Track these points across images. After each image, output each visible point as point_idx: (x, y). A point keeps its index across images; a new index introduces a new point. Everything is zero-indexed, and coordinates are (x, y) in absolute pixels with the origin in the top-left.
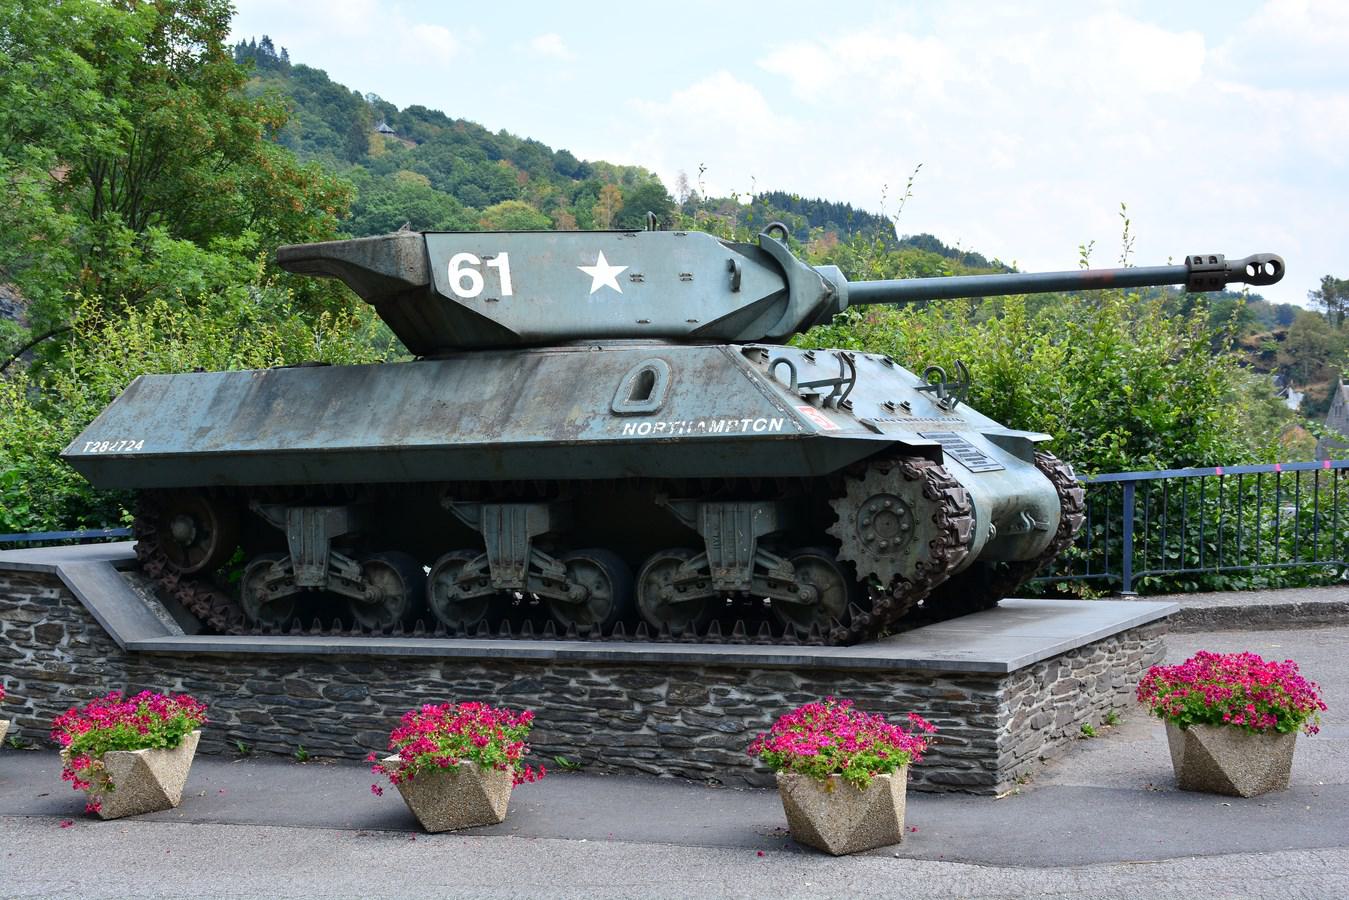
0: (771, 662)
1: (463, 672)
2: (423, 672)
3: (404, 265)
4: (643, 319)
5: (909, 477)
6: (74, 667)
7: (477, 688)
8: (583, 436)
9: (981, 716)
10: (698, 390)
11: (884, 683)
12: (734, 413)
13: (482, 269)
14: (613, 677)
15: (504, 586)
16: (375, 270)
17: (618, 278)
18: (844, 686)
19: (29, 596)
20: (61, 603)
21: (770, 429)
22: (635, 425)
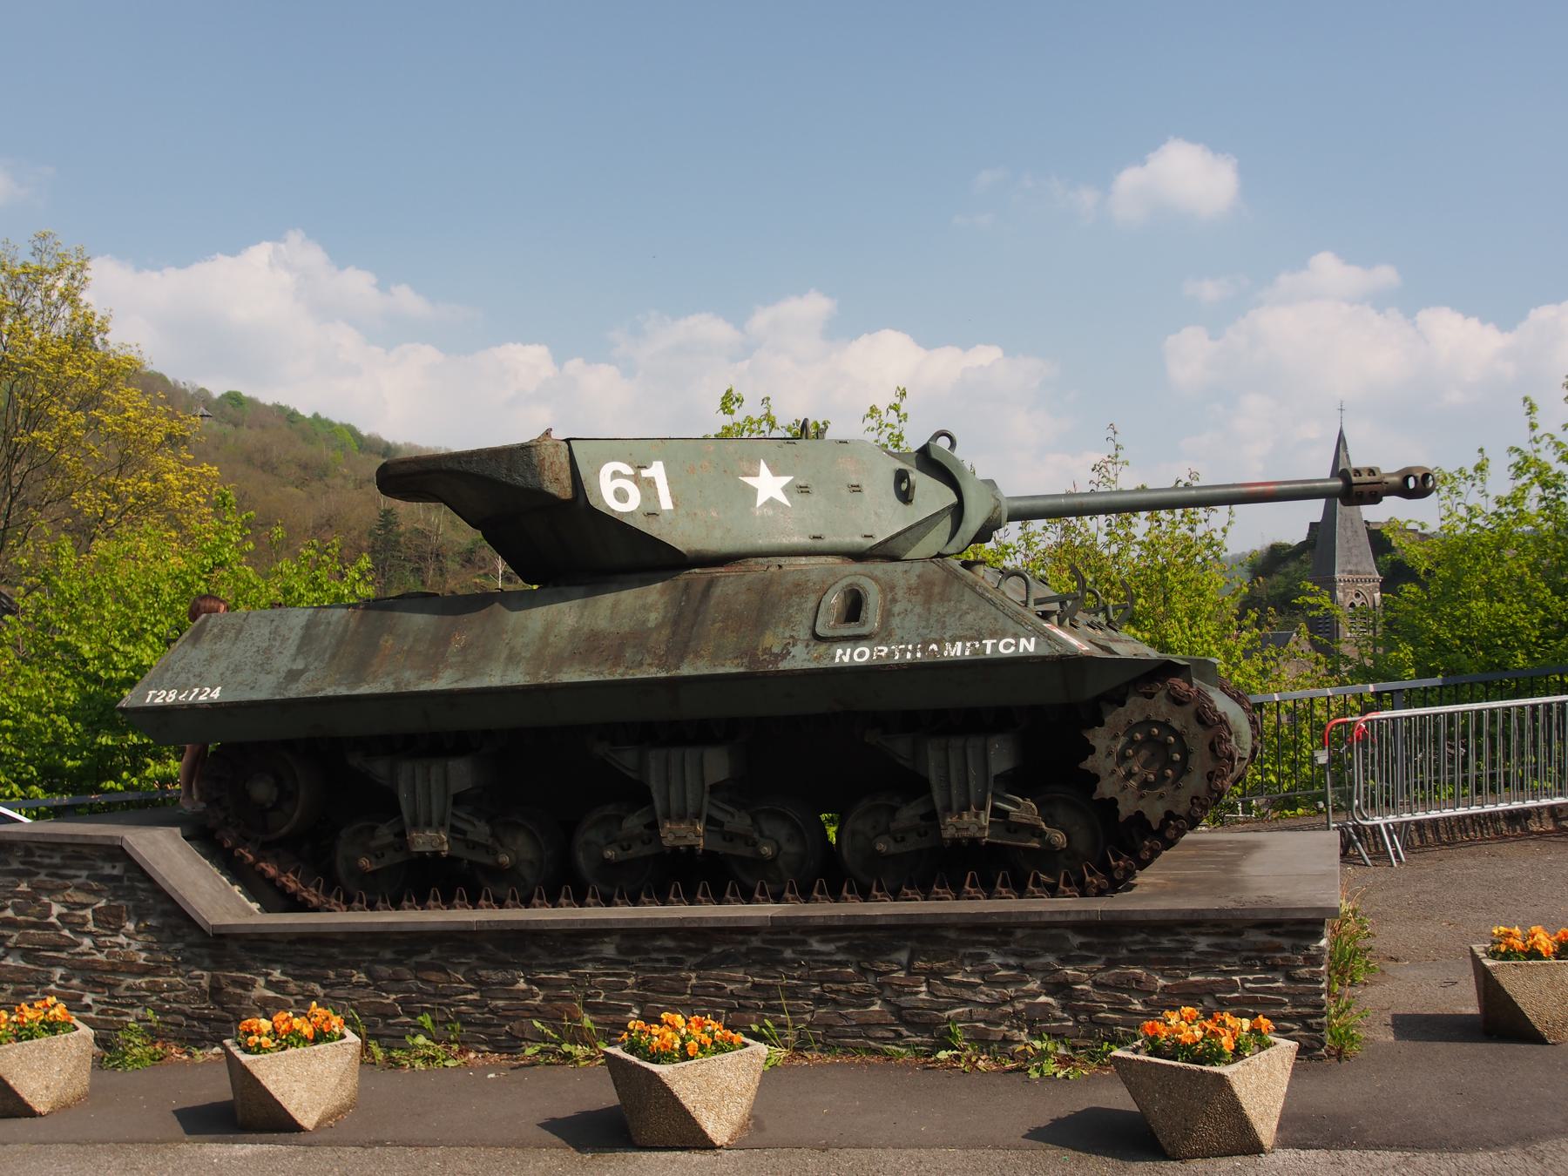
0: (1046, 918)
1: (646, 946)
2: (594, 948)
3: (548, 476)
4: (817, 534)
5: (1177, 701)
6: (144, 955)
7: (665, 965)
8: (784, 665)
9: (1304, 970)
10: (918, 609)
11: (1184, 937)
12: (969, 633)
13: (636, 479)
14: (839, 944)
15: (677, 843)
16: (512, 483)
17: (786, 490)
18: (1135, 943)
19: (85, 873)
20: (125, 879)
21: (1021, 650)
22: (849, 651)
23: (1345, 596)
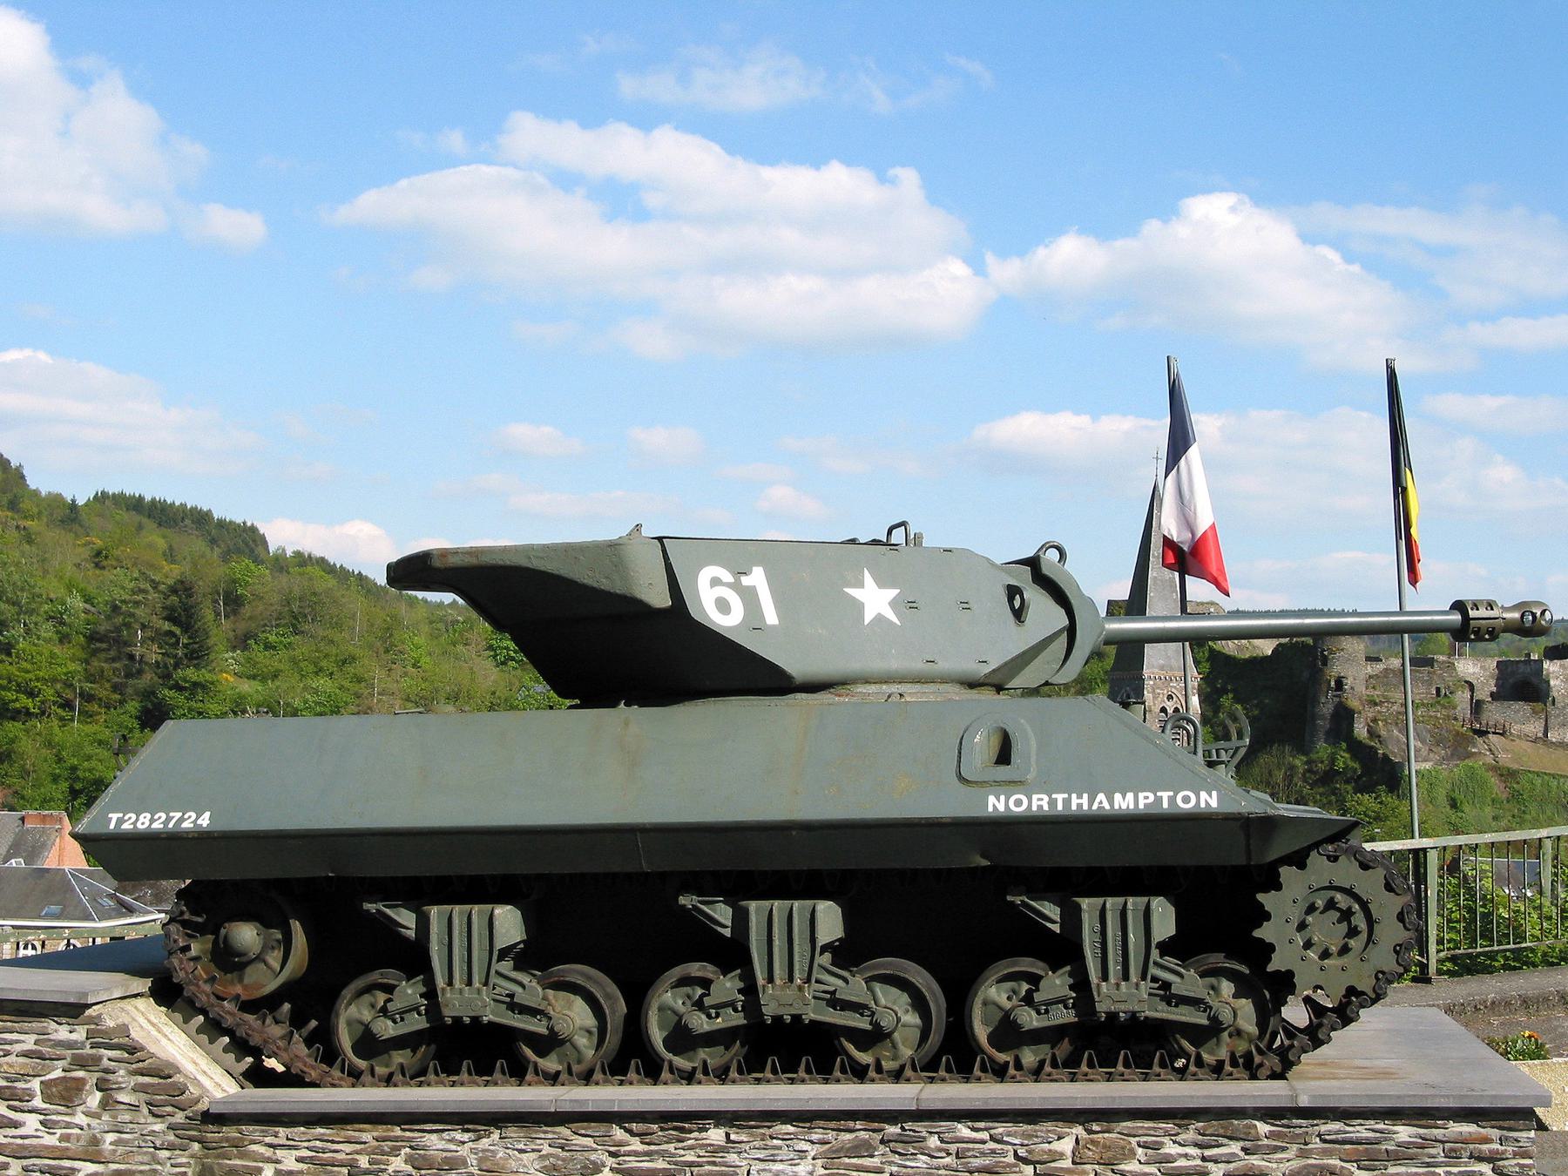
6: (110, 1137)
13: (736, 587)
21: (1203, 805)
23: (1155, 698)
